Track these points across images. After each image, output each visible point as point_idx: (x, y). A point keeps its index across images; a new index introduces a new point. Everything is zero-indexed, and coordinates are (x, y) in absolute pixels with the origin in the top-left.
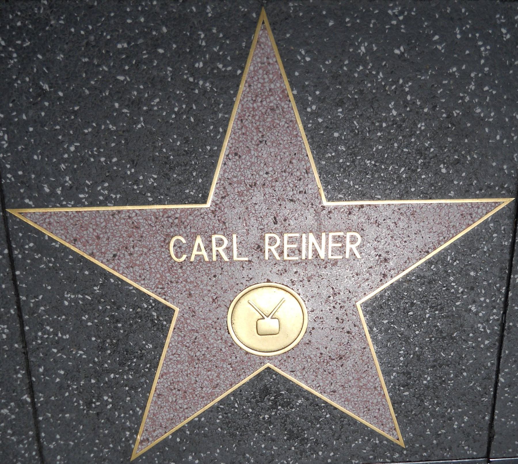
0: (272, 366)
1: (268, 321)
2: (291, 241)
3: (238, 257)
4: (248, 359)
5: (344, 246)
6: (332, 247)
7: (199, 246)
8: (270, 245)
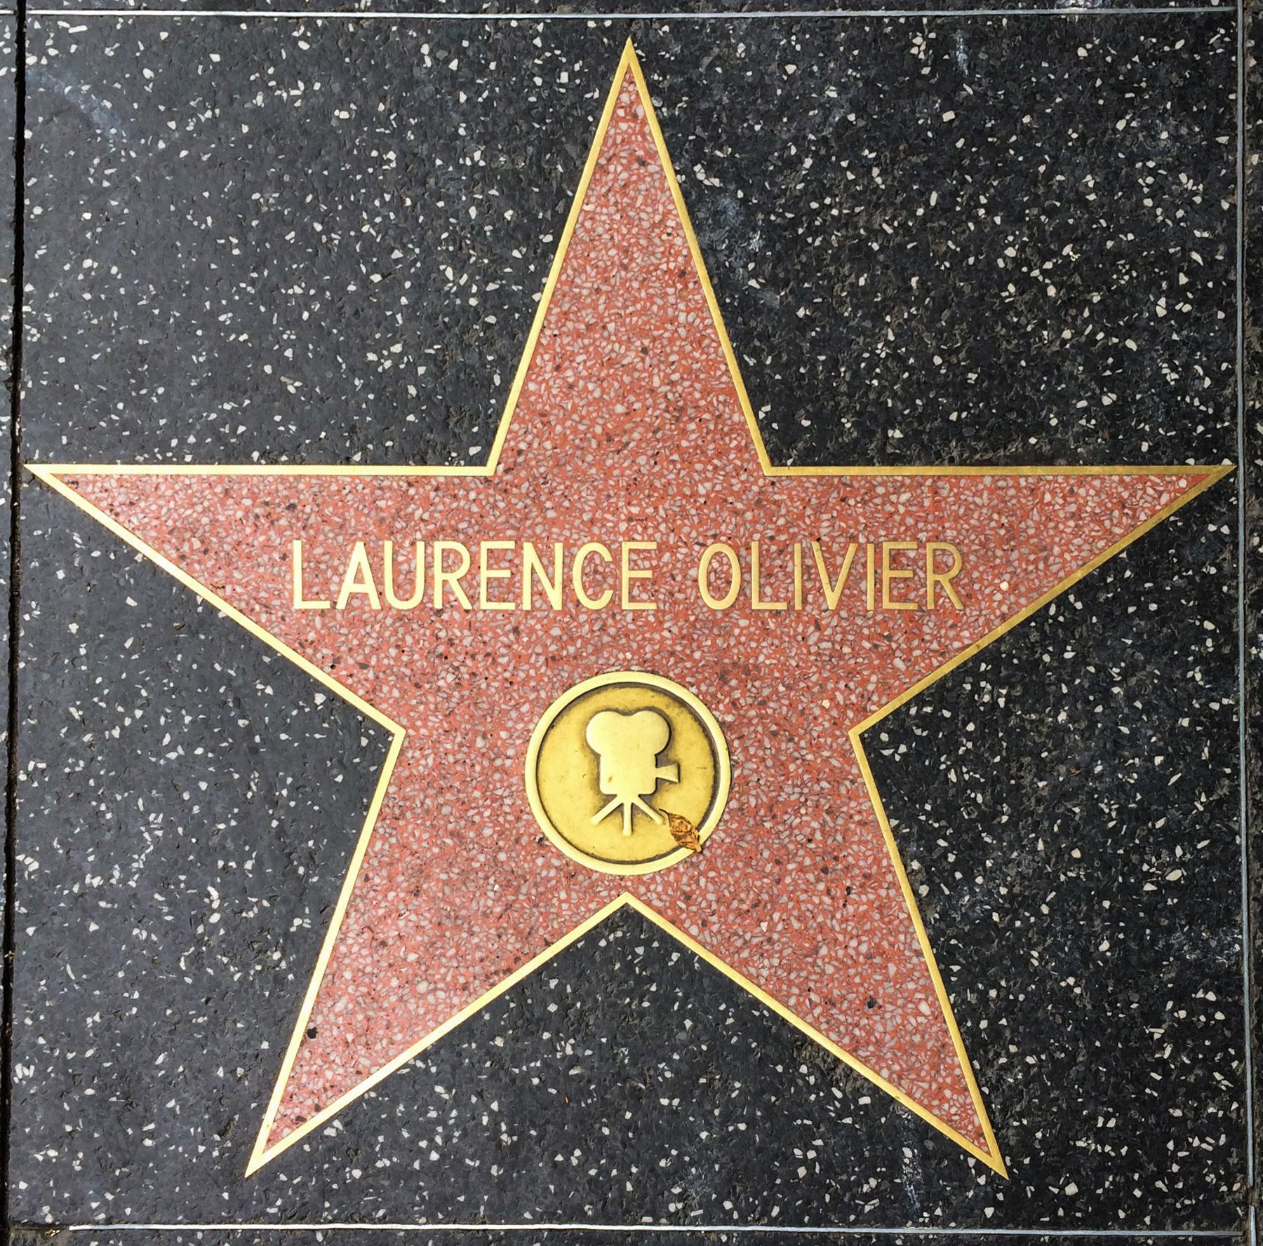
1: (612, 792)
2: (495, 558)
7: (359, 571)
8: (444, 570)
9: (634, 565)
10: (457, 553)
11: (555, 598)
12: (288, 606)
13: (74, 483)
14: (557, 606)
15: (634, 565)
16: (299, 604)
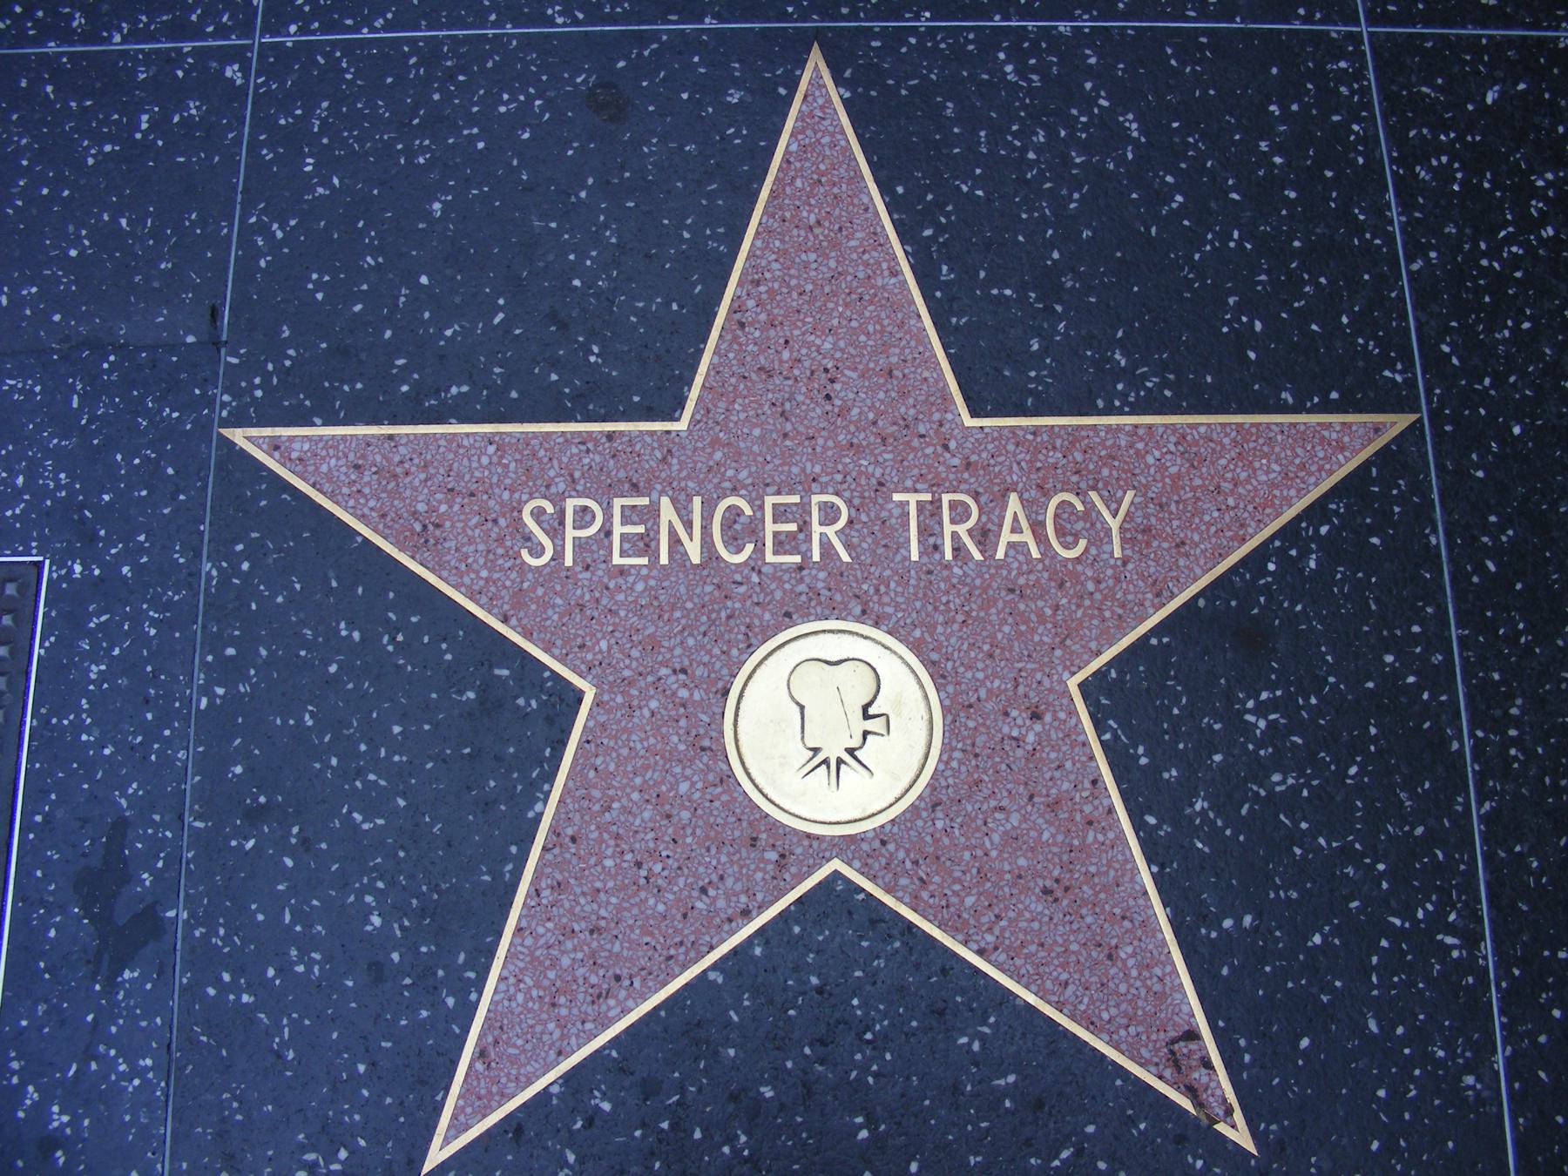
0: (1081, 676)
1: (833, 736)
2: (780, 514)
3: (775, 553)
4: (788, 848)
5: (805, 527)
6: (776, 534)
8: (953, 522)
9: (625, 521)
10: (963, 503)
11: (694, 552)
12: (607, 560)
13: (1377, 430)
14: (695, 558)
15: (625, 521)
16: (617, 560)
